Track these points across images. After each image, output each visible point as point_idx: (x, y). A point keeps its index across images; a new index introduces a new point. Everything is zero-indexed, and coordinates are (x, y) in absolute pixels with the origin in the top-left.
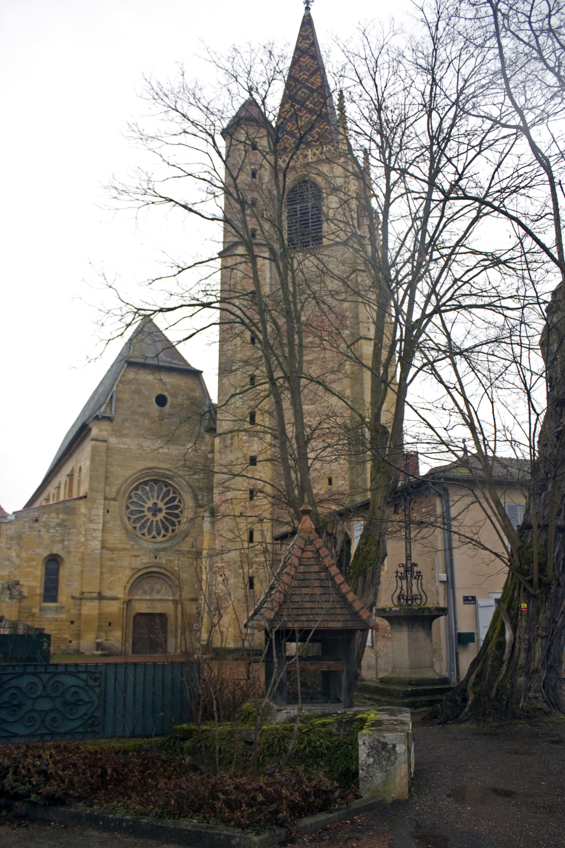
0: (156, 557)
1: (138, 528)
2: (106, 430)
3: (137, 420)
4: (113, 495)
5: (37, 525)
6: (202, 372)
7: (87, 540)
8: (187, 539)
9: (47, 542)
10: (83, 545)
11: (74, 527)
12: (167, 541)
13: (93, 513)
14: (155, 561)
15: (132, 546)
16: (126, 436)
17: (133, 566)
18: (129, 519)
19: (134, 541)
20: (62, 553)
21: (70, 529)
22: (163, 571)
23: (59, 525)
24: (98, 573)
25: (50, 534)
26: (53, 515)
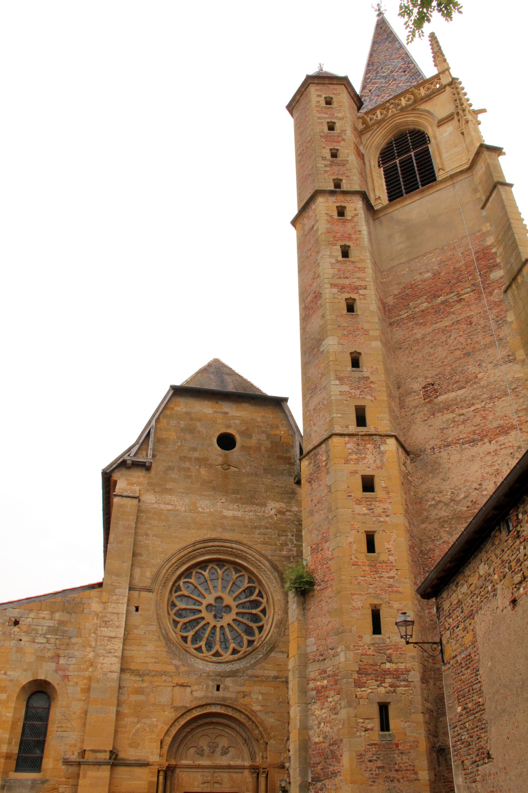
0: (218, 688)
1: (189, 639)
2: (139, 484)
3: (188, 469)
4: (147, 583)
5: (16, 629)
6: (286, 400)
7: (97, 655)
8: (273, 654)
9: (30, 658)
10: (92, 665)
11: (79, 635)
12: (239, 659)
13: (110, 610)
14: (216, 693)
15: (177, 667)
16: (169, 491)
17: (178, 704)
18: (176, 623)
19: (180, 660)
20: (54, 679)
21: (70, 638)
22: (230, 713)
23: (53, 630)
24: (113, 715)
25: (36, 646)
26: (45, 614)
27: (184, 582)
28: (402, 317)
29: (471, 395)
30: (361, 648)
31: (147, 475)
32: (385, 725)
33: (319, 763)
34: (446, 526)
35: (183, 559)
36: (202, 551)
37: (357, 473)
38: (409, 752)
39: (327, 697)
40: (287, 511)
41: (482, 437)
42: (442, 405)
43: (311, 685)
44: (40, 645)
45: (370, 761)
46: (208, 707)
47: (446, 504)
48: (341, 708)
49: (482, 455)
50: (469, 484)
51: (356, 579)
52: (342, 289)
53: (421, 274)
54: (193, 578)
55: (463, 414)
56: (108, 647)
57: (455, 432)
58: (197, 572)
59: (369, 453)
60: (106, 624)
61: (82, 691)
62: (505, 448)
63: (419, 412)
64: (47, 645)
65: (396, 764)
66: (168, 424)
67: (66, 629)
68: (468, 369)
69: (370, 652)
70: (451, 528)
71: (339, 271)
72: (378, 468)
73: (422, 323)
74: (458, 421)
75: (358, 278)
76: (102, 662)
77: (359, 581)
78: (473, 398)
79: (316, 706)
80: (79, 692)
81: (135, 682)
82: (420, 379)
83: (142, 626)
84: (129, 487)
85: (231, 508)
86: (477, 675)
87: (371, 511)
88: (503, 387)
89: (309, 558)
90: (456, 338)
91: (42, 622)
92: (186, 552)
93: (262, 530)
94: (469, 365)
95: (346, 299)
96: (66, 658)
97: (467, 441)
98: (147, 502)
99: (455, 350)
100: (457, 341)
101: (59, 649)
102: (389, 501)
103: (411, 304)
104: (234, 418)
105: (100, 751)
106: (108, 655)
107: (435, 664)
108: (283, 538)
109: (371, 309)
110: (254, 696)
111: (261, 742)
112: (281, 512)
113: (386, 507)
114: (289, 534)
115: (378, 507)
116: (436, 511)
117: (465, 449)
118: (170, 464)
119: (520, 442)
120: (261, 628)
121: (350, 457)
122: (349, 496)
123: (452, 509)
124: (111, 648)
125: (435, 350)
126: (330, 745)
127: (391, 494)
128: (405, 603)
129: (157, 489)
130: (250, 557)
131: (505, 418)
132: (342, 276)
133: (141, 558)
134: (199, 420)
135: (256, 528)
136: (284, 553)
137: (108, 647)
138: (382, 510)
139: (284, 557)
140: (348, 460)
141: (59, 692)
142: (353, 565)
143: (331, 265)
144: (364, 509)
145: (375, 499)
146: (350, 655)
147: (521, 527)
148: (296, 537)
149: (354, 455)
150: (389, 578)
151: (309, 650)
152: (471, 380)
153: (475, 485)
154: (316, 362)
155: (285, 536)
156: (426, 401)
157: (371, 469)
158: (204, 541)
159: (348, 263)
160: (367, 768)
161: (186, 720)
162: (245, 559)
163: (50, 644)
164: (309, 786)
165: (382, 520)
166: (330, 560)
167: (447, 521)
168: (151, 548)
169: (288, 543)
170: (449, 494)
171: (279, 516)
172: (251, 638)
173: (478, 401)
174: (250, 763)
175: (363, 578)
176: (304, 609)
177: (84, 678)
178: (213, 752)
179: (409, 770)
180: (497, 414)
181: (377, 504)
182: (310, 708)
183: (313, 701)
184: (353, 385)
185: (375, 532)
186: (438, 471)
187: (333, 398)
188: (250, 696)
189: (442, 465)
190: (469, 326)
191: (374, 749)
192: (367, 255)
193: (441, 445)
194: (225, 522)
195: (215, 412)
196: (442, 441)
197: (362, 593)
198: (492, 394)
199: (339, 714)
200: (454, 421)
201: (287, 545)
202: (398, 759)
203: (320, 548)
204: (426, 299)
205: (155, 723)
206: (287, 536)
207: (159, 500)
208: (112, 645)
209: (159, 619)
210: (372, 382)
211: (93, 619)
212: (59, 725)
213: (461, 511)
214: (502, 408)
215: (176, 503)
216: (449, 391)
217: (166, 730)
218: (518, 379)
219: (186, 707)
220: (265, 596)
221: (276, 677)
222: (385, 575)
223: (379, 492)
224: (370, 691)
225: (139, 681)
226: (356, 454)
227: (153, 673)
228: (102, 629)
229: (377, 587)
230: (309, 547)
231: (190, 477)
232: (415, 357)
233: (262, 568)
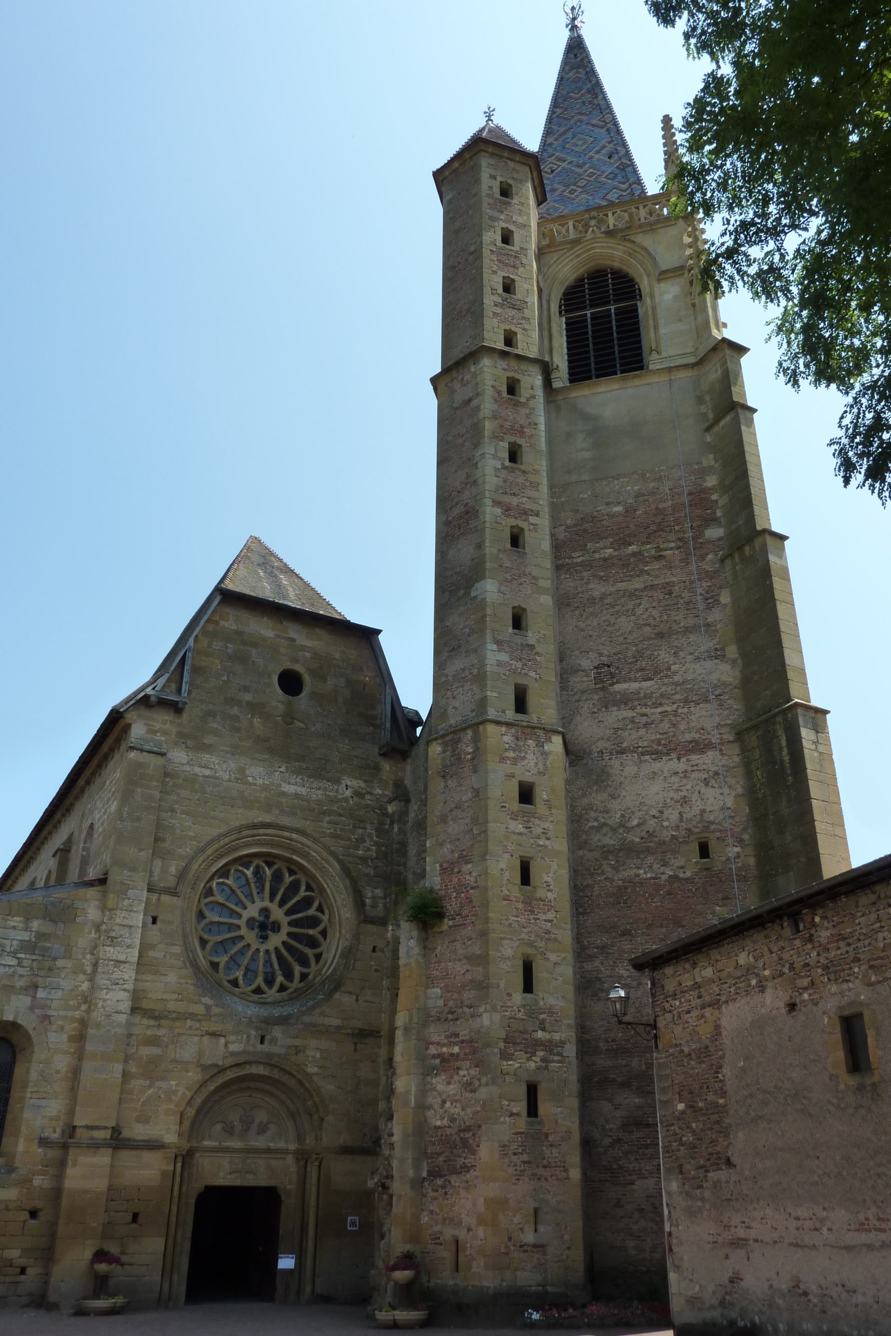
2: (165, 733)
3: (236, 718)
8: (337, 996)
11: (68, 955)
13: (118, 921)
14: (260, 1047)
16: (203, 748)
21: (55, 959)
23: (28, 947)
27: (218, 884)
28: (575, 560)
29: (660, 692)
30: (509, 1010)
31: (177, 721)
32: (532, 1110)
33: (442, 1153)
34: (611, 858)
35: (222, 850)
36: (249, 841)
37: (514, 777)
38: (560, 1145)
39: (458, 1069)
40: (368, 793)
41: (670, 750)
42: (618, 696)
43: (433, 1050)
44: (7, 969)
45: (515, 1154)
46: (248, 1067)
47: (614, 830)
48: (480, 1085)
49: (666, 774)
50: (646, 808)
51: (507, 919)
52: (507, 510)
53: (608, 504)
54: (231, 877)
55: (646, 715)
56: (114, 976)
57: (633, 737)
58: (236, 870)
59: (529, 752)
60: (112, 941)
61: (71, 1039)
62: (697, 770)
63: (587, 700)
64: (19, 969)
65: (544, 1159)
66: (210, 645)
67: (48, 945)
68: (659, 655)
69: (519, 1015)
70: (617, 861)
71: (505, 481)
72: (539, 773)
73: (603, 577)
74: (639, 723)
75: (529, 498)
76: (105, 997)
77: (510, 922)
78: (662, 696)
79: (438, 1079)
80: (66, 1040)
81: (148, 1027)
82: (592, 655)
83: (161, 946)
84: (150, 736)
85: (293, 781)
86: (718, 1073)
87: (528, 830)
88: (704, 690)
89: (438, 879)
90: (647, 609)
91: (12, 934)
92: (227, 840)
93: (335, 818)
94: (661, 650)
95: (512, 527)
96: (47, 990)
97: (648, 751)
98: (175, 761)
99: (645, 625)
100: (648, 613)
101: (37, 975)
102: (551, 819)
103: (589, 545)
104: (303, 648)
105: (98, 1128)
106: (114, 987)
107: (584, 1033)
108: (360, 831)
109: (543, 547)
110: (310, 1053)
111: (315, 1117)
112: (358, 794)
113: (546, 827)
114: (368, 826)
115: (537, 825)
116: (597, 837)
117: (645, 761)
118: (210, 706)
119: (718, 766)
120: (318, 957)
121: (507, 754)
122: (503, 807)
123: (620, 837)
124: (119, 977)
125: (616, 619)
126: (459, 1131)
127: (554, 811)
128: (563, 955)
129: (190, 743)
130: (314, 854)
131: (702, 731)
132: (508, 490)
133: (163, 845)
134: (254, 645)
135: (324, 813)
136: (360, 852)
137: (114, 976)
138: (542, 831)
139: (360, 858)
140: (503, 758)
141: (35, 1040)
142: (505, 900)
143: (495, 470)
144: (521, 826)
145: (533, 815)
146: (497, 1017)
147: (817, 931)
148: (376, 831)
149: (512, 752)
150: (545, 921)
151: (431, 1003)
152: (662, 671)
153: (654, 812)
154: (462, 609)
155: (363, 828)
156: (597, 686)
157: (530, 774)
158: (255, 826)
159: (517, 471)
160: (511, 1162)
161: (218, 1084)
162: (306, 856)
163: (23, 967)
164: (423, 1182)
165: (541, 843)
166: (472, 888)
167: (612, 852)
168: (178, 831)
169: (367, 839)
170: (618, 816)
171: (356, 799)
172: (305, 970)
173: (667, 702)
174: (296, 1145)
175: (515, 919)
176: (425, 948)
177: (73, 1020)
178: (247, 1130)
179: (559, 1167)
180: (692, 724)
181: (537, 821)
182: (430, 1080)
183: (435, 1072)
184: (514, 654)
185: (532, 858)
186: (605, 783)
187: (489, 668)
188: (304, 1053)
189: (611, 776)
190: (667, 597)
191: (520, 1139)
192: (543, 464)
193: (612, 749)
194: (284, 801)
195: (278, 636)
196: (614, 744)
197: (514, 938)
198: (688, 696)
199: (477, 1093)
200: (633, 722)
201: (365, 841)
202: (547, 1152)
203: (456, 870)
204: (612, 544)
205: (174, 1088)
206: (365, 828)
207: (192, 760)
208: (120, 973)
209: (185, 936)
210: (537, 653)
211: (90, 933)
212: (35, 1089)
213: (632, 841)
214: (700, 717)
215: (216, 767)
216: (630, 680)
217: (189, 1098)
218: (724, 684)
219: (216, 1065)
220: (326, 911)
221: (338, 1028)
222: (542, 917)
223: (540, 808)
224: (517, 1065)
225: (154, 1026)
226: (514, 751)
227: (174, 1016)
228: (107, 948)
229: (531, 932)
230: (438, 865)
231: (238, 730)
232: (589, 622)
233: (329, 872)
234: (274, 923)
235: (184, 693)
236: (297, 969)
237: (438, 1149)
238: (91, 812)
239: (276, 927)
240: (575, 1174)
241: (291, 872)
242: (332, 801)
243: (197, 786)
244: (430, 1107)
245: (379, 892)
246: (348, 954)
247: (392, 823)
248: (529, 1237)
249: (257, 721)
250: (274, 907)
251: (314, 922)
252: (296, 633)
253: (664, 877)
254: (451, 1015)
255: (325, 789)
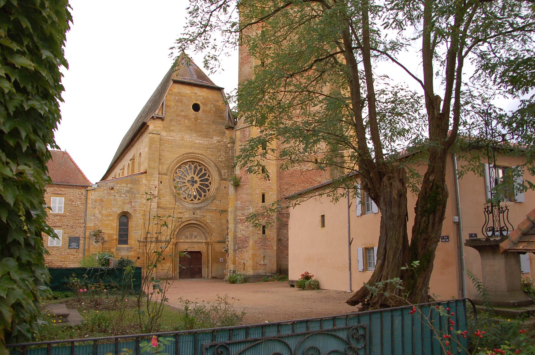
2: (159, 127)
3: (180, 121)
8: (214, 201)
21: (135, 195)
32: (264, 232)
43: (238, 218)
84: (155, 129)
85: (198, 139)
104: (200, 96)
108: (220, 153)
120: (209, 190)
134: (184, 96)
151: (237, 205)
162: (204, 161)
172: (205, 194)
177: (142, 210)
221: (216, 210)
231: (181, 124)
234: (195, 181)
235: (164, 115)
236: (203, 194)
237: (240, 242)
238: (140, 149)
239: (196, 182)
240: (275, 248)
241: (200, 166)
242: (211, 144)
243: (170, 143)
244: (238, 232)
245: (226, 171)
246: (217, 189)
247: (229, 150)
248: (262, 263)
249: (186, 121)
250: (195, 176)
251: (207, 180)
252: (197, 90)
253: (304, 169)
254: (243, 209)
255: (208, 141)
